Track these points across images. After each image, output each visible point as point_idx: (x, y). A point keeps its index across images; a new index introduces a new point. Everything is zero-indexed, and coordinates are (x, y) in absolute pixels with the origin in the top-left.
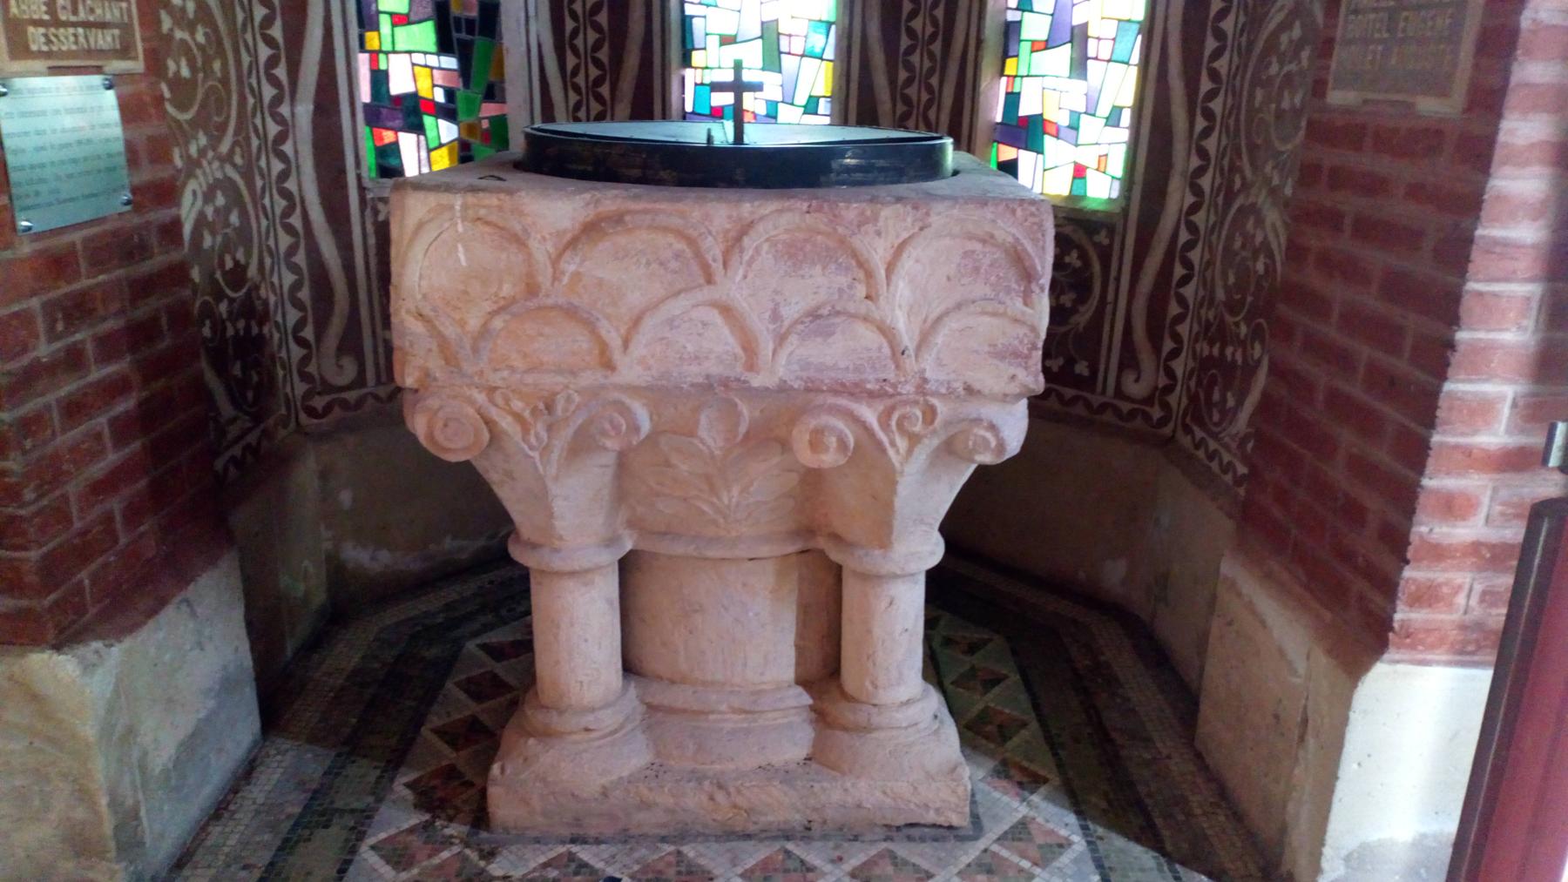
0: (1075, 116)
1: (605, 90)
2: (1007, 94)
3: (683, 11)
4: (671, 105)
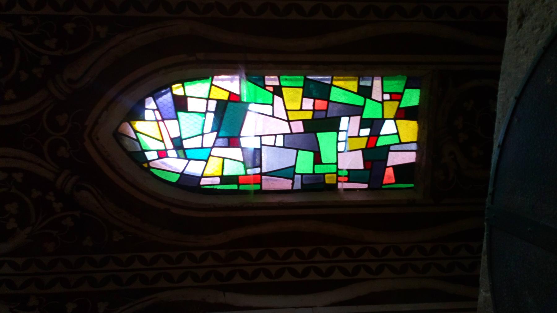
0: (364, 124)
1: (355, 248)
2: (349, 181)
3: (297, 191)
4: (363, 201)
